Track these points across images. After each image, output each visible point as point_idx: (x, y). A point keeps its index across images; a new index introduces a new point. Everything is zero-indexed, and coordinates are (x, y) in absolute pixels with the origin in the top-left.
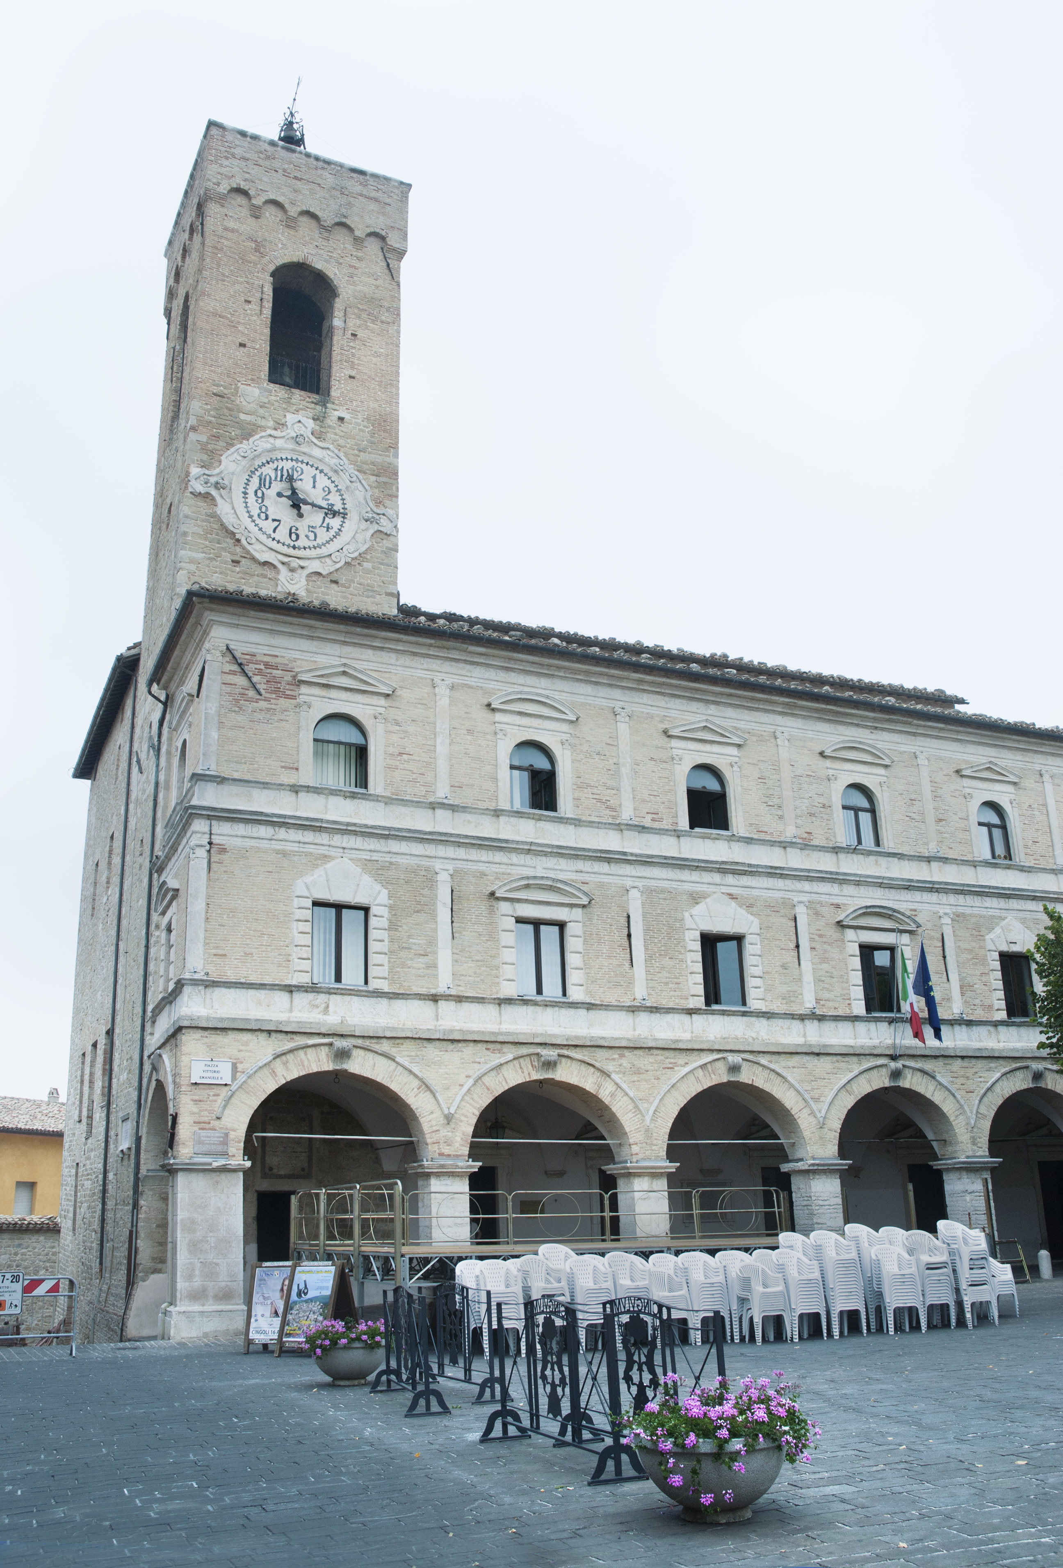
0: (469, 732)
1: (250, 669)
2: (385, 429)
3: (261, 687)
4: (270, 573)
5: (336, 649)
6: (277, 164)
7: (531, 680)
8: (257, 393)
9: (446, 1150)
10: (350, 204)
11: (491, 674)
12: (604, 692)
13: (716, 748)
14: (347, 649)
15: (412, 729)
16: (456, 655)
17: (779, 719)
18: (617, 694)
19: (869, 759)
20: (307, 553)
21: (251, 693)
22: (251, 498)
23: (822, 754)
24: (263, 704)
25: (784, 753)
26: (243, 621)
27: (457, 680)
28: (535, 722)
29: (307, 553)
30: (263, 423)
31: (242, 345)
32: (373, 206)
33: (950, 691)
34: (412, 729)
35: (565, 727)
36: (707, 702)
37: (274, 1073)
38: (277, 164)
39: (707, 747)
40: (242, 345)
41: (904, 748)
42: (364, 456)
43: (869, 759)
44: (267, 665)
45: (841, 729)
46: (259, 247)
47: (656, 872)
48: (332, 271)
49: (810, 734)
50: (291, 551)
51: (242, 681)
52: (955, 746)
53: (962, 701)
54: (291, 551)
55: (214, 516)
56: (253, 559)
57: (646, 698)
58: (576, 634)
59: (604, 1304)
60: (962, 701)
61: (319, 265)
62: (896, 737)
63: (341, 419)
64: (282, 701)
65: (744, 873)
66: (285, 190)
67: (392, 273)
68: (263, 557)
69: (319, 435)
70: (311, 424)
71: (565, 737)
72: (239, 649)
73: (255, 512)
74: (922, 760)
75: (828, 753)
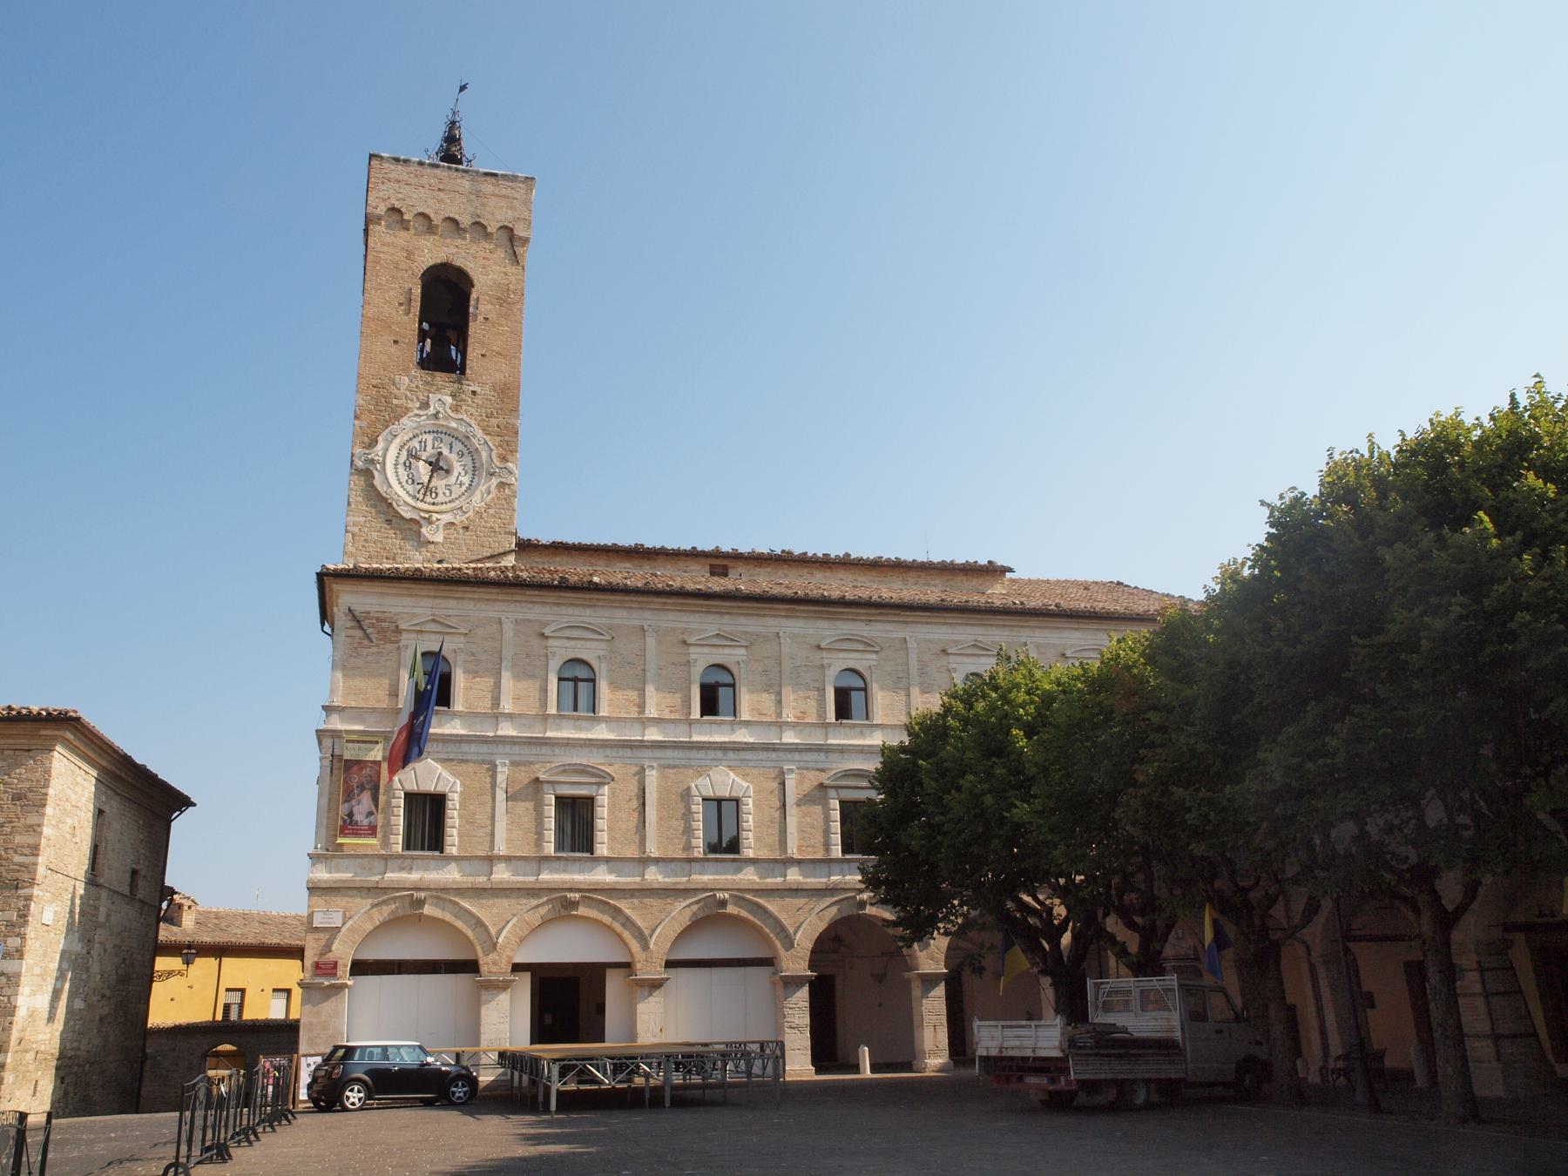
0: (528, 656)
1: (365, 624)
2: (508, 395)
3: (373, 637)
4: (415, 528)
5: (428, 602)
6: (424, 181)
7: (577, 611)
8: (409, 381)
9: (494, 969)
10: (483, 205)
11: (547, 609)
12: (635, 614)
13: (727, 651)
14: (438, 601)
15: (483, 657)
16: (518, 598)
17: (784, 622)
18: (647, 614)
19: (861, 647)
20: (444, 507)
21: (366, 642)
22: (401, 469)
23: (819, 647)
24: (374, 649)
25: (785, 650)
26: (360, 588)
27: (520, 617)
28: (580, 644)
29: (444, 507)
30: (410, 405)
31: (396, 342)
32: (503, 203)
33: (1000, 561)
34: (483, 657)
35: (603, 645)
36: (722, 613)
37: (371, 918)
38: (424, 181)
39: (720, 651)
40: (396, 342)
41: (895, 635)
42: (494, 421)
43: (861, 647)
44: (378, 620)
45: (839, 624)
46: (410, 256)
47: (669, 753)
48: (471, 267)
49: (811, 631)
50: (431, 508)
51: (359, 633)
52: (945, 629)
53: (1011, 570)
54: (431, 508)
55: (373, 486)
56: (402, 518)
57: (671, 616)
58: (663, 548)
59: (337, 1048)
60: (1011, 570)
61: (458, 263)
62: (889, 627)
63: (474, 393)
64: (388, 646)
65: (743, 749)
66: (431, 202)
67: (515, 259)
68: (407, 515)
69: (456, 409)
70: (449, 400)
71: (601, 653)
72: (359, 609)
73: (404, 478)
74: (912, 645)
75: (823, 645)
